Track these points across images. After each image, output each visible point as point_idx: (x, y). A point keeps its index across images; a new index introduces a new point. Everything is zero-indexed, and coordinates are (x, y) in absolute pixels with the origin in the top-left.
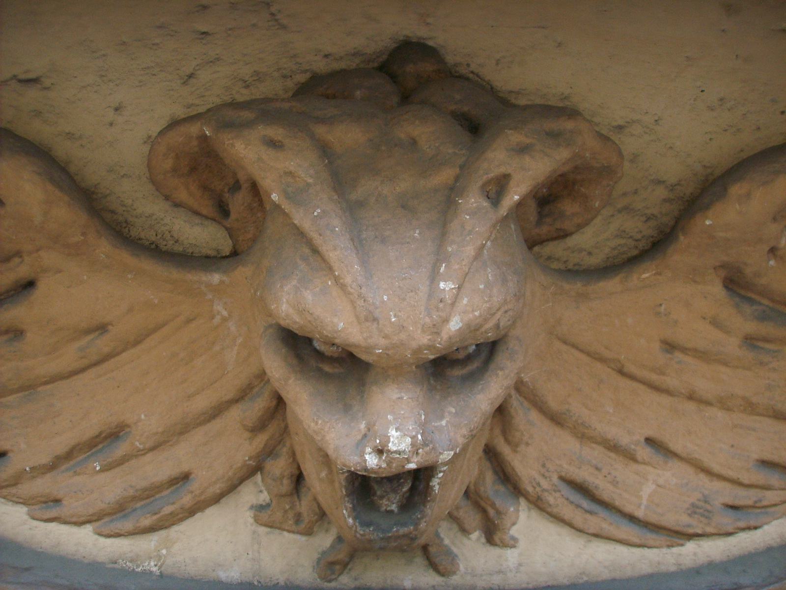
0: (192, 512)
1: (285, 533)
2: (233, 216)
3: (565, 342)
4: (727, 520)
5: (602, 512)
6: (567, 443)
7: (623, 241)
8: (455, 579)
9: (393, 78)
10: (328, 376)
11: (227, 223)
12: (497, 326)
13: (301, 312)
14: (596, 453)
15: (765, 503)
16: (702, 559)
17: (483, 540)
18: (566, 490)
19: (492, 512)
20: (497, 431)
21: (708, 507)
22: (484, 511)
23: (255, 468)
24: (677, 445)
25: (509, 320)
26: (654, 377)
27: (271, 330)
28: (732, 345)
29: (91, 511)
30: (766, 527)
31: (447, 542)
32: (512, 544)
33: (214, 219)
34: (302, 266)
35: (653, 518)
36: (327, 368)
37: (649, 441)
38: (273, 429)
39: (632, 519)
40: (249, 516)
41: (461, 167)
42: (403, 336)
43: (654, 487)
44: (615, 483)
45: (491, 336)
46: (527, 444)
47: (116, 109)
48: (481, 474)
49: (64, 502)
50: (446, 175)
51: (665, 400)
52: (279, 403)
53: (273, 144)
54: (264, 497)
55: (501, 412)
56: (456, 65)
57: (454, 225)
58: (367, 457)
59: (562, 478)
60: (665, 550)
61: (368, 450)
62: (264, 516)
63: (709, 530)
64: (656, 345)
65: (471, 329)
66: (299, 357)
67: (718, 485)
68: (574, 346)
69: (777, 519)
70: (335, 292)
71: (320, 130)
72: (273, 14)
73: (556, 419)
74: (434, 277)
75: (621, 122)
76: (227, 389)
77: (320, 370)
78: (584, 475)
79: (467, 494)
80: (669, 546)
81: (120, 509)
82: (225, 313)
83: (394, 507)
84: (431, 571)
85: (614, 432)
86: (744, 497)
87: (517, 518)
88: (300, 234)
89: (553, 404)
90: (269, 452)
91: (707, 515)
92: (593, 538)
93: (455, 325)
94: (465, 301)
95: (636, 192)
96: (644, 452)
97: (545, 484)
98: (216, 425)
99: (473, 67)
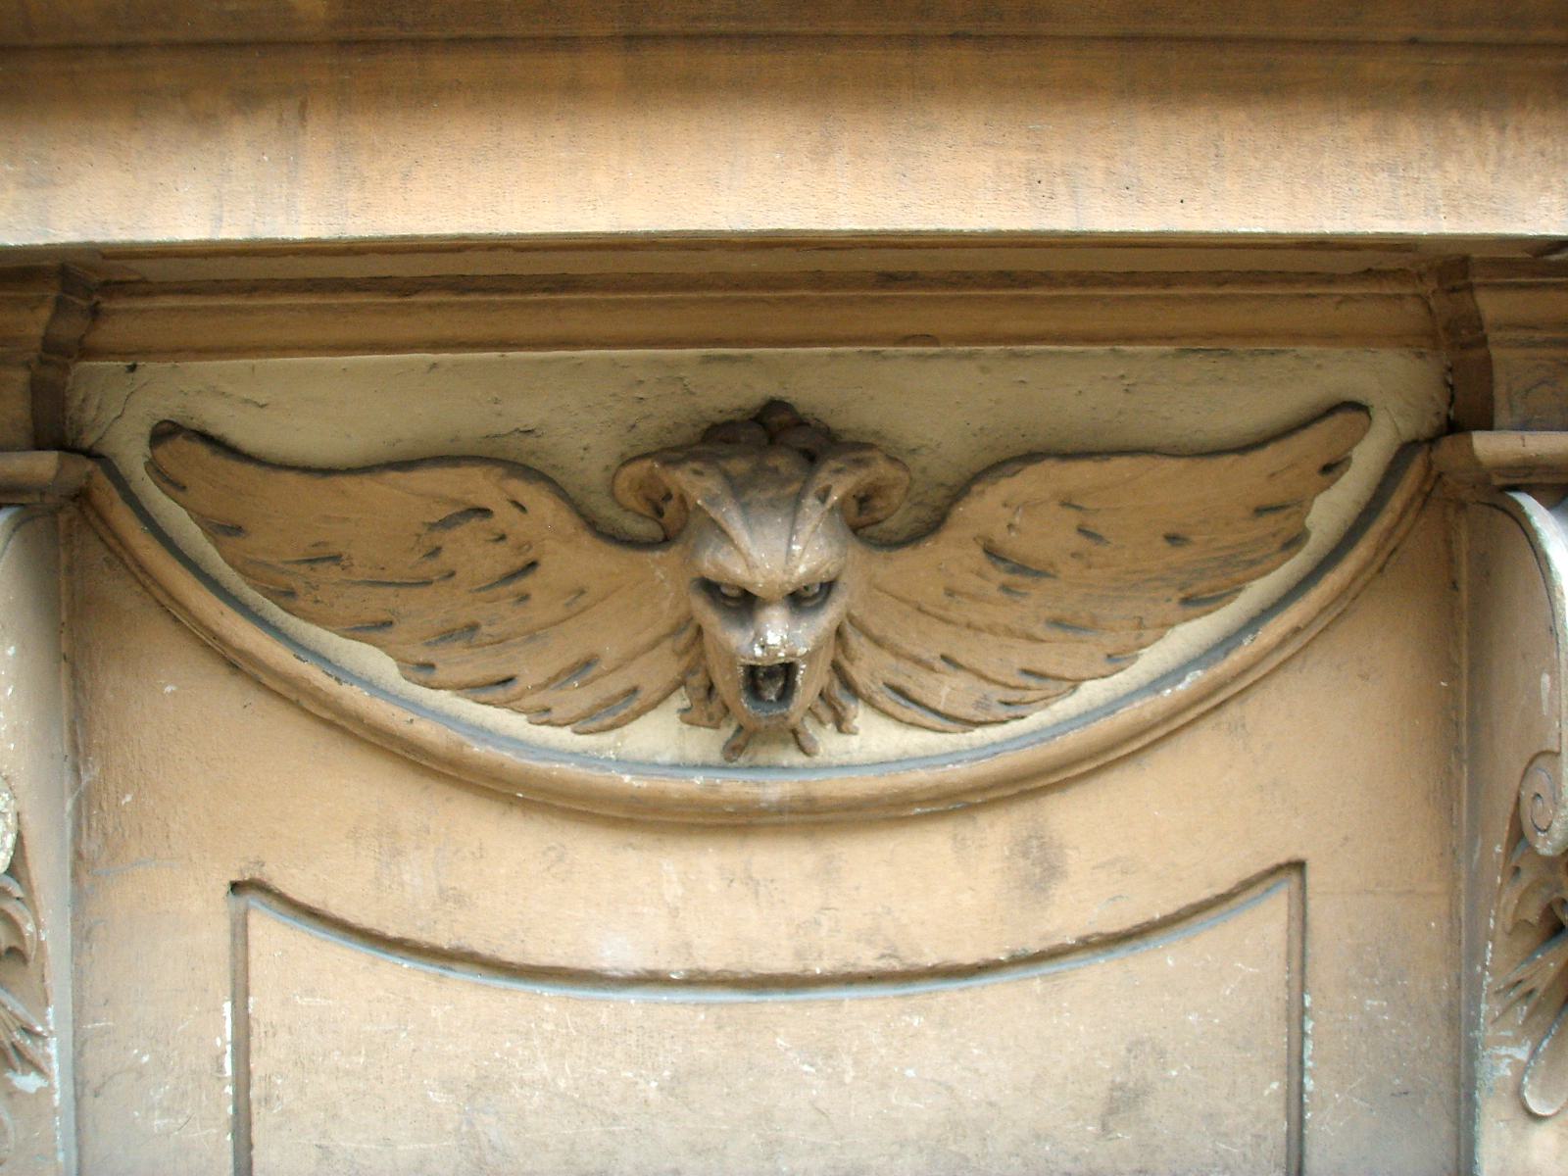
0: (638, 714)
1: (702, 729)
2: (666, 515)
3: (880, 590)
4: (1002, 712)
5: (915, 708)
6: (888, 659)
7: (918, 524)
8: (818, 759)
9: (764, 426)
10: (730, 608)
11: (661, 521)
12: (827, 572)
13: (716, 566)
14: (907, 666)
15: (1026, 700)
16: (987, 741)
17: (835, 729)
18: (889, 692)
19: (839, 709)
20: (839, 650)
21: (987, 702)
22: (834, 709)
23: (681, 683)
24: (962, 659)
25: (421, 118)
26: (942, 612)
27: (695, 583)
28: (992, 590)
29: (572, 715)
30: (1031, 717)
31: (810, 732)
32: (853, 732)
33: (652, 519)
34: (717, 540)
35: (950, 711)
36: (730, 603)
37: (944, 658)
38: (694, 652)
39: (937, 713)
40: (676, 717)
41: (805, 482)
42: (774, 576)
43: (948, 690)
44: (922, 687)
45: (825, 578)
46: (860, 659)
47: (585, 449)
48: (831, 683)
49: (553, 711)
50: (795, 487)
51: (950, 628)
52: (699, 631)
53: (697, 473)
54: (687, 703)
55: (839, 633)
56: (804, 414)
57: (800, 515)
58: (756, 649)
59: (887, 685)
60: (961, 735)
61: (756, 645)
62: (688, 716)
63: (989, 718)
64: (941, 591)
65: (813, 572)
66: (713, 597)
67: (994, 687)
68: (886, 592)
69: (1039, 710)
70: (735, 553)
71: (722, 463)
72: (685, 385)
73: (878, 642)
74: (790, 543)
75: (913, 447)
76: (663, 627)
77: (724, 604)
78: (900, 681)
79: (821, 695)
80: (964, 732)
81: (589, 715)
82: (662, 577)
83: (773, 698)
84: (801, 753)
85: (917, 651)
86: (1014, 695)
87: (857, 713)
88: (714, 522)
89: (876, 632)
90: (690, 671)
91: (987, 708)
92: (910, 727)
93: (802, 569)
94: (808, 556)
95: (926, 492)
96: (939, 664)
97: (874, 687)
98: (656, 652)
99: (816, 416)
